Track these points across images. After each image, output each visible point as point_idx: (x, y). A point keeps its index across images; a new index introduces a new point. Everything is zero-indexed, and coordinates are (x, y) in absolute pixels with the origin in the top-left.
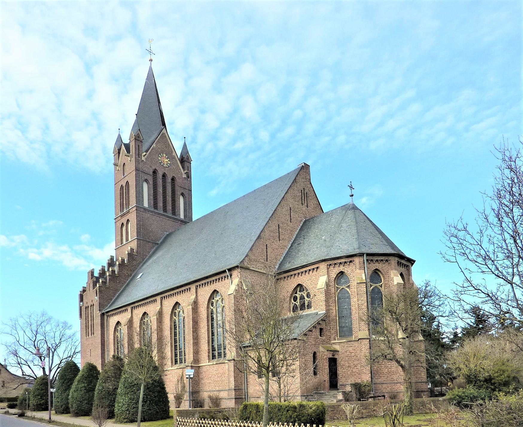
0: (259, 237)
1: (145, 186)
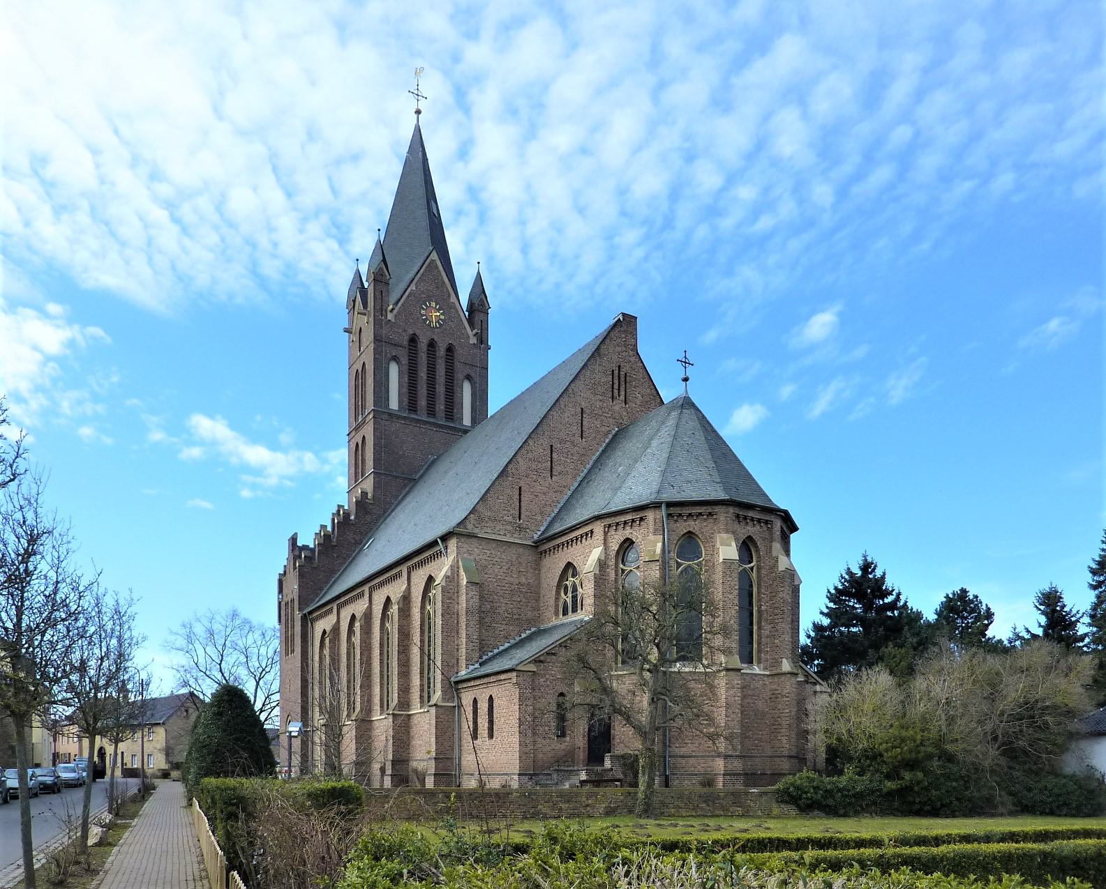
0: (503, 473)
1: (394, 370)
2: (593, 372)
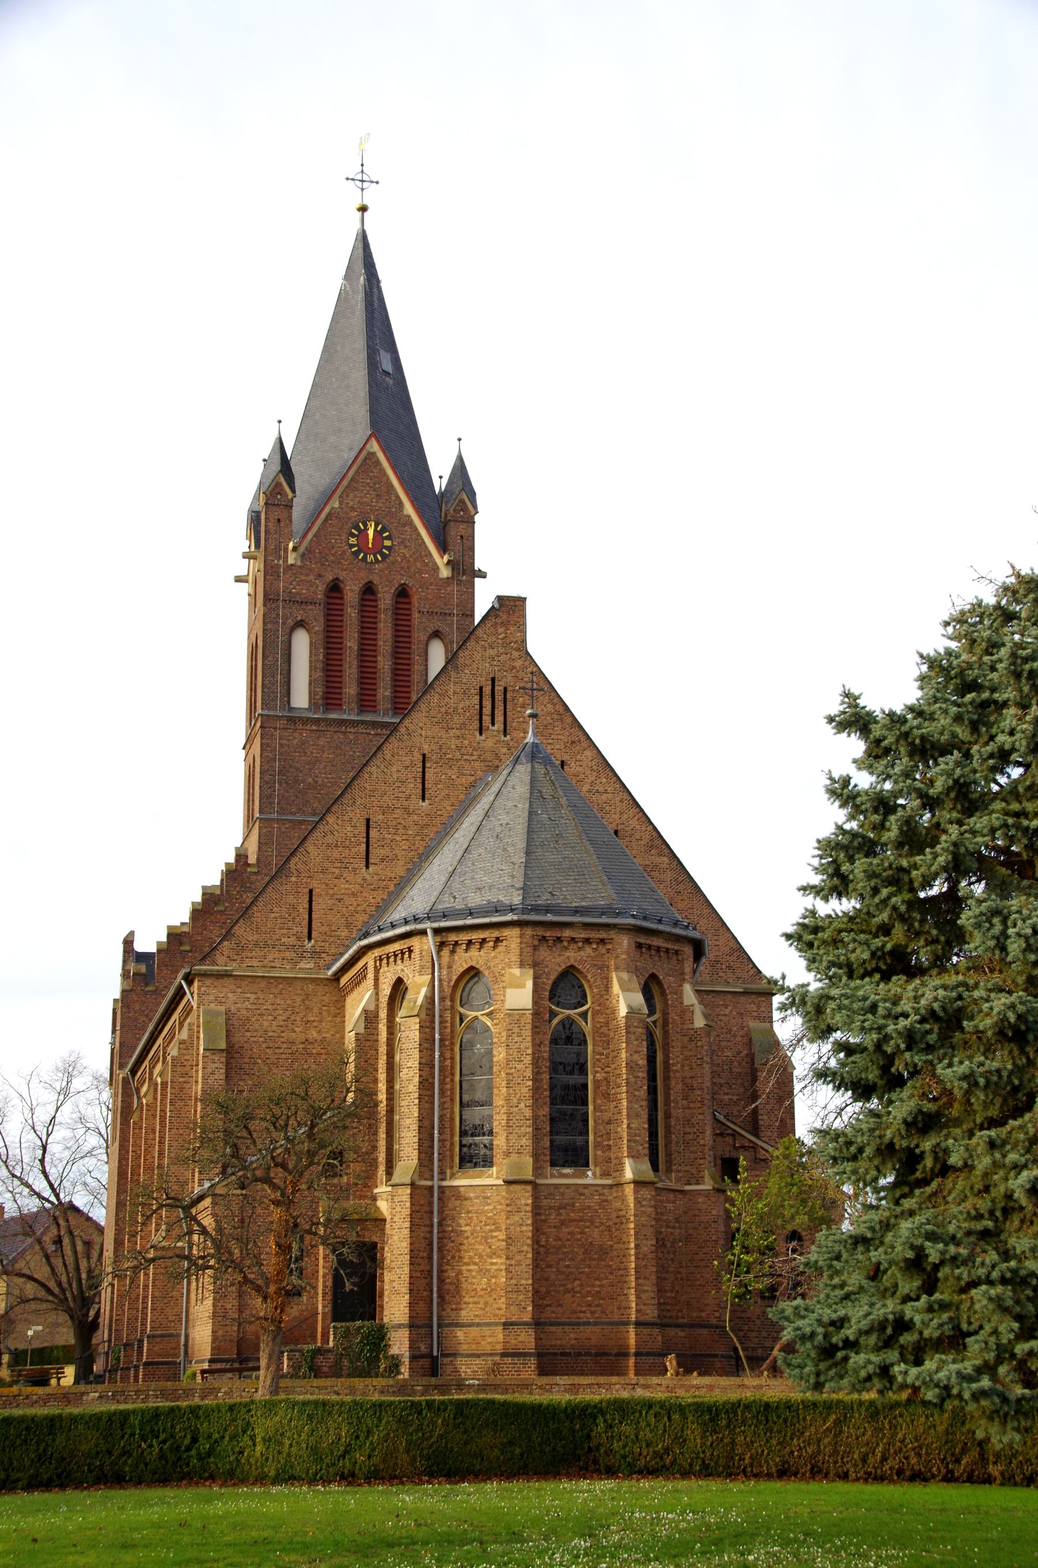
1: (301, 644)
2: (443, 695)
